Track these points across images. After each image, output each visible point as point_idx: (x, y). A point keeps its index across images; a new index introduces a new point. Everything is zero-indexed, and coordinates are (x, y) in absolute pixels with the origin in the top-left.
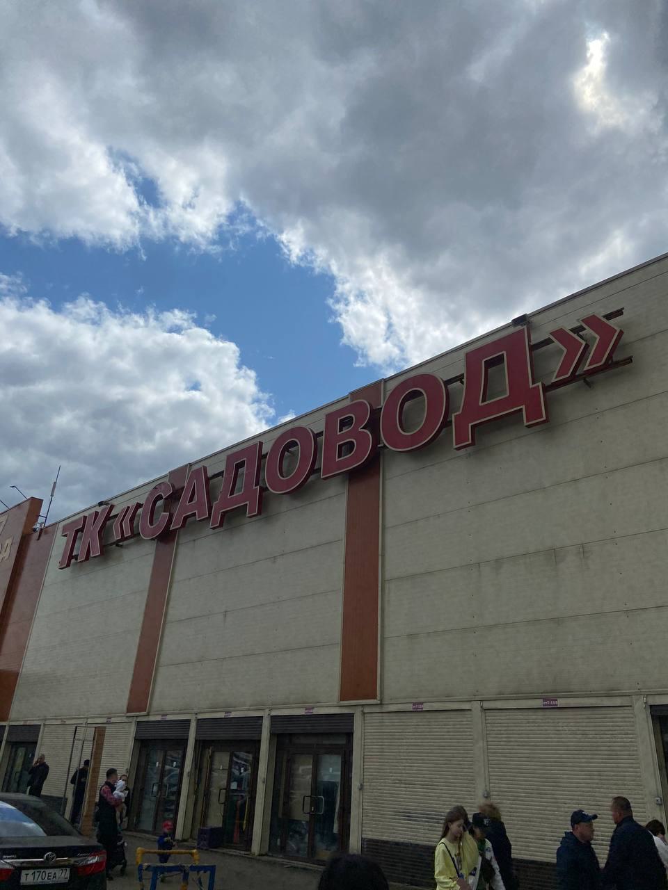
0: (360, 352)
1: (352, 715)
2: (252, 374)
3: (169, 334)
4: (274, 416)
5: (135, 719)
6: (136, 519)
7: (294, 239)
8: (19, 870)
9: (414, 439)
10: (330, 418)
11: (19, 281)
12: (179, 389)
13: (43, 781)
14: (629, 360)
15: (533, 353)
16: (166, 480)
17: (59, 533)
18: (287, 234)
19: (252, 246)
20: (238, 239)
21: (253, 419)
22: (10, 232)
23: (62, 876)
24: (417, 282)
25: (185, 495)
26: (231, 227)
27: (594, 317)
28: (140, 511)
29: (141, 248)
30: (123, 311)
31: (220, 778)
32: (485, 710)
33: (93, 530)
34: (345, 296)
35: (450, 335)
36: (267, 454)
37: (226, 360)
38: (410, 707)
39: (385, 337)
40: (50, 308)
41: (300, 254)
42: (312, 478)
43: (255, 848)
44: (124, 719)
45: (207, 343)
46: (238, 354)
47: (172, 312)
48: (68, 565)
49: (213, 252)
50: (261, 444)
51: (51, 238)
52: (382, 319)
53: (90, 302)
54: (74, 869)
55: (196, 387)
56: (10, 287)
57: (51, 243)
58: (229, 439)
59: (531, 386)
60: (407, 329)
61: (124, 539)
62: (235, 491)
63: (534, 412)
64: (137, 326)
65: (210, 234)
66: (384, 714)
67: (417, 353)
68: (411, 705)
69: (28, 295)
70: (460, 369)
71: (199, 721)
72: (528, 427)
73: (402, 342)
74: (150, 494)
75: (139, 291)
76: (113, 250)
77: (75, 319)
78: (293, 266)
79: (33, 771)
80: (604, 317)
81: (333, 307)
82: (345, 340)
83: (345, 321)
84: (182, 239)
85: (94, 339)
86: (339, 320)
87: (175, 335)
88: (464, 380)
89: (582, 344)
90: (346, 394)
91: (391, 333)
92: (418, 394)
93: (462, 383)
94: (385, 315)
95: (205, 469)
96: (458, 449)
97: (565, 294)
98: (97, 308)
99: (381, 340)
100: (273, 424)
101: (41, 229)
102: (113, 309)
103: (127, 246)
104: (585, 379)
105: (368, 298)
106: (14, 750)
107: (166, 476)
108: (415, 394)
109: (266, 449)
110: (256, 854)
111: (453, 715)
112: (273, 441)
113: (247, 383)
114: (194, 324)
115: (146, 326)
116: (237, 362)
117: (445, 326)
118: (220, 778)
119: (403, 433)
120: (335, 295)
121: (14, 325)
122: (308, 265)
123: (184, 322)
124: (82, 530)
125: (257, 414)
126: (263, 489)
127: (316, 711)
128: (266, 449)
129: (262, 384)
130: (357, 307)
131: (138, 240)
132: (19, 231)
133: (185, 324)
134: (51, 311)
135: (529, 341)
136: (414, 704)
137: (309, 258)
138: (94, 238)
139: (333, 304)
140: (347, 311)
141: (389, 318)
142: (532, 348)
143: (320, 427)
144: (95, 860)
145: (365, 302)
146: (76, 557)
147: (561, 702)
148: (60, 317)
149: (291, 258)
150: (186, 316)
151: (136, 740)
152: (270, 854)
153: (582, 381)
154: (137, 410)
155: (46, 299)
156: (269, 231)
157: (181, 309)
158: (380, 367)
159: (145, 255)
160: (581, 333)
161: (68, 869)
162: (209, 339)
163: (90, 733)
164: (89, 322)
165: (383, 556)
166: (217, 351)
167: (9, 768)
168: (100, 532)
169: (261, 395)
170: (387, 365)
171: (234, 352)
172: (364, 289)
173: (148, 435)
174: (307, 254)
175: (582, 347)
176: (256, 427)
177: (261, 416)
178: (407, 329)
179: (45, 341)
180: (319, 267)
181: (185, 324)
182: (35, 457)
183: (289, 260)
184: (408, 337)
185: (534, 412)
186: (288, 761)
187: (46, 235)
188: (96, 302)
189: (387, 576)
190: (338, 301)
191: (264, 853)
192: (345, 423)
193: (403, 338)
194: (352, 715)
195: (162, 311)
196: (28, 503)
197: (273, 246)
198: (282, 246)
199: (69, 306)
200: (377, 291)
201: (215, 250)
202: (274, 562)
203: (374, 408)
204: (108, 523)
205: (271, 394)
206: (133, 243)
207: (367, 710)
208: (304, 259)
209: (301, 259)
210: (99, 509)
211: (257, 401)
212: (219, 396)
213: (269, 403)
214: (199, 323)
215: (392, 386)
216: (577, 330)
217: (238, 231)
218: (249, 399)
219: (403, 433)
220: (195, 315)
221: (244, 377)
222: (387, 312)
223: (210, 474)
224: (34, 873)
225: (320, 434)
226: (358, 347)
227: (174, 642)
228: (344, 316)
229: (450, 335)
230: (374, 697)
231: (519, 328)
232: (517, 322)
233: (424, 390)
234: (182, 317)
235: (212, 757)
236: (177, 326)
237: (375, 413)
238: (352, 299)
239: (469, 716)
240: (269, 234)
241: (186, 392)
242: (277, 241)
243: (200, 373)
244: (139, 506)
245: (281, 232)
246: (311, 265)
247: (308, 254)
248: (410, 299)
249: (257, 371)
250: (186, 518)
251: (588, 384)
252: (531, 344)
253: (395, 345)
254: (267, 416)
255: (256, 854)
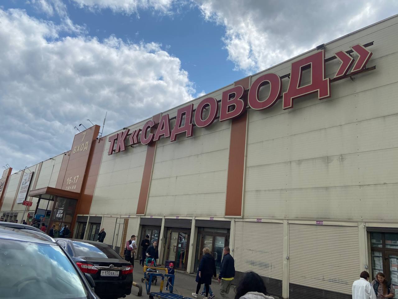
0: (236, 64)
1: (230, 222)
2: (186, 73)
3: (149, 54)
4: (195, 93)
5: (140, 216)
6: (139, 136)
7: (207, 8)
8: (100, 271)
9: (264, 104)
10: (224, 94)
11: (85, 29)
12: (154, 79)
13: (104, 239)
14: (374, 68)
15: (326, 63)
16: (151, 119)
17: (108, 140)
18: (204, 5)
19: (188, 11)
20: (181, 8)
21: (186, 94)
22: (80, 6)
23: (117, 274)
24: (266, 29)
25: (160, 127)
26: (178, 2)
27: (358, 45)
28: (141, 132)
29: (138, 13)
30: (129, 42)
31: (174, 243)
32: (289, 224)
33: (121, 139)
34: (230, 36)
35: (280, 55)
36: (195, 110)
37: (175, 66)
38: (256, 220)
39: (248, 56)
40: (98, 41)
41: (210, 15)
42: (215, 121)
43: (188, 270)
44: (135, 217)
45: (166, 58)
46: (180, 64)
47: (151, 44)
48: (112, 154)
49: (170, 15)
50: (193, 105)
51: (98, 8)
52: (247, 47)
53: (115, 38)
54: (121, 271)
55: (161, 78)
56: (81, 31)
57: (98, 11)
58: (176, 103)
59: (323, 80)
60: (259, 52)
61: (134, 144)
62: (181, 126)
63: (324, 92)
64: (136, 50)
65: (168, 6)
66: (244, 222)
67: (263, 64)
68: (256, 219)
69: (88, 35)
70: (289, 71)
71: (166, 219)
72: (320, 99)
73: (256, 59)
74: (145, 126)
75: (137, 33)
76: (125, 14)
77: (109, 46)
78: (206, 21)
79: (100, 234)
80: (363, 46)
81: (224, 42)
82: (229, 58)
83: (230, 48)
84: (156, 8)
85: (117, 56)
86: (227, 48)
87: (152, 54)
88: (290, 77)
89: (351, 59)
90: (233, 82)
91: (251, 54)
92: (267, 83)
93: (289, 78)
94: (249, 46)
95: (168, 115)
96: (284, 109)
97: (340, 36)
98: (118, 41)
99: (246, 58)
100: (195, 96)
101: (94, 4)
102: (125, 41)
103: (131, 12)
104: (351, 76)
105: (241, 37)
106: (92, 226)
107: (151, 118)
108: (266, 83)
109: (195, 107)
110: (189, 273)
111: (273, 225)
112: (199, 104)
113: (184, 77)
114: (160, 49)
115: (140, 50)
116: (180, 67)
117: (278, 51)
118: (174, 243)
119: (259, 101)
120: (225, 36)
121: (84, 49)
122: (213, 21)
123: (156, 48)
124: (117, 139)
125: (188, 92)
126: (193, 125)
127: (215, 219)
128: (195, 107)
129: (190, 78)
130: (236, 41)
131: (136, 9)
132: (84, 5)
133: (157, 49)
134: (99, 43)
135: (325, 57)
136: (257, 219)
137: (214, 17)
138: (117, 8)
139: (156, 49)
140: (231, 44)
141: (251, 47)
142: (326, 61)
143: (219, 97)
144: (129, 269)
145: (240, 39)
146: (115, 151)
147: (324, 223)
148: (102, 45)
149: (206, 18)
150: (157, 45)
151: (140, 225)
152: (195, 273)
153: (349, 78)
154: (136, 88)
155: (96, 37)
156: (196, 4)
157: (155, 42)
158: (245, 71)
159: (139, 16)
160: (351, 54)
161: (119, 272)
162: (167, 56)
163: (123, 221)
164: (115, 48)
165: (246, 156)
166: (171, 62)
167: (90, 233)
168: (124, 141)
169: (190, 83)
170: (249, 70)
171: (178, 63)
172: (240, 33)
173: (141, 100)
174: (213, 15)
175: (352, 60)
176: (187, 98)
177: (189, 93)
178: (259, 52)
179: (97, 56)
180: (219, 22)
181: (157, 49)
182: (94, 107)
183: (205, 18)
184: (259, 56)
185: (324, 92)
186: (202, 238)
187: (96, 7)
188: (118, 38)
189: (248, 165)
190: (227, 39)
191: (192, 273)
192: (232, 96)
193: (257, 57)
194: (230, 222)
195: (146, 43)
196: (95, 127)
197: (197, 11)
198: (201, 11)
199: (106, 40)
200: (246, 34)
201: (171, 13)
202: (198, 157)
203: (246, 90)
204: (127, 137)
205: (195, 83)
206: (134, 11)
207: (236, 220)
208: (212, 17)
209: (210, 18)
210: (124, 131)
211: (188, 86)
212: (171, 83)
213: (193, 87)
214: (163, 48)
215: (254, 79)
216: (349, 52)
217: (181, 4)
218: (185, 85)
219: (259, 101)
220: (161, 45)
221: (183, 74)
222: (250, 44)
223: (170, 118)
224: (106, 272)
225: (220, 101)
226: (235, 62)
227: (155, 188)
228: (229, 46)
229: (280, 55)
230: (240, 215)
231: (320, 51)
232: (319, 48)
233: (241, 85)
234: (155, 46)
235: (171, 234)
236: (153, 50)
237: (246, 92)
238: (233, 37)
239: (282, 226)
240: (195, 5)
241: (157, 81)
242: (199, 9)
243: (163, 72)
244: (140, 130)
245: (201, 4)
246: (215, 21)
247: (214, 14)
248: (261, 38)
249: (189, 72)
250: (160, 136)
251: (352, 79)
252: (326, 59)
253: (253, 60)
254: (192, 93)
255: (189, 273)
